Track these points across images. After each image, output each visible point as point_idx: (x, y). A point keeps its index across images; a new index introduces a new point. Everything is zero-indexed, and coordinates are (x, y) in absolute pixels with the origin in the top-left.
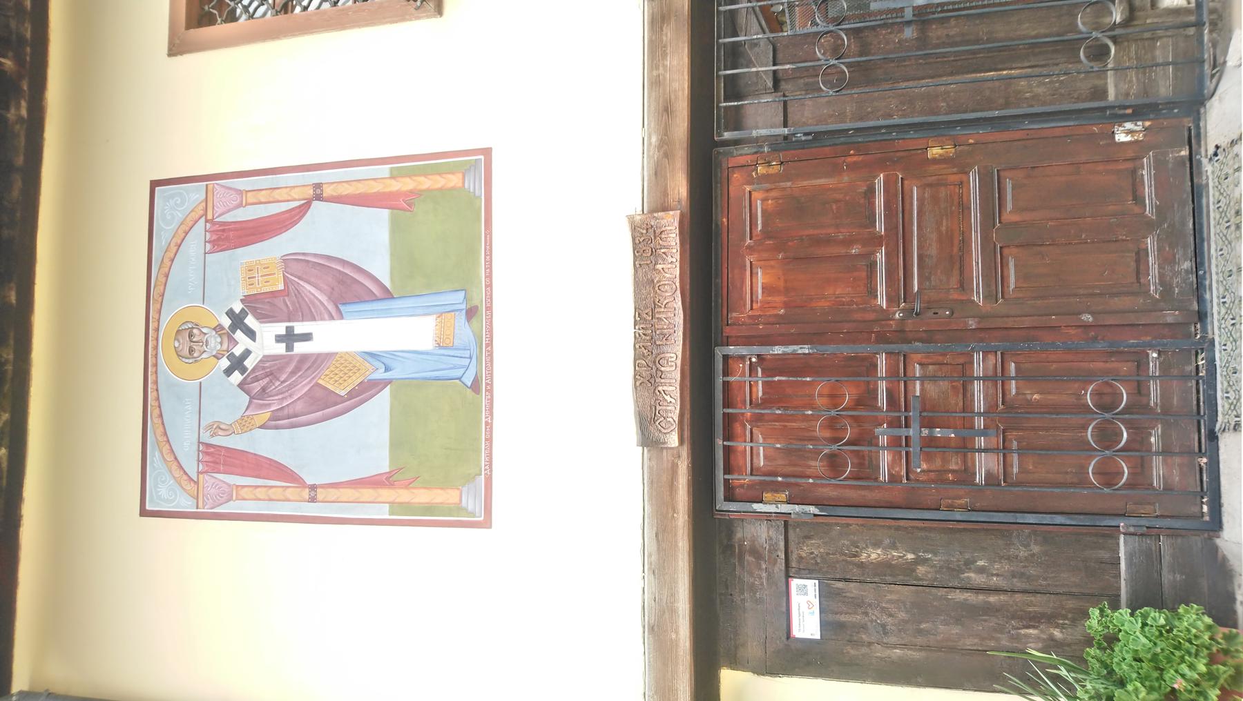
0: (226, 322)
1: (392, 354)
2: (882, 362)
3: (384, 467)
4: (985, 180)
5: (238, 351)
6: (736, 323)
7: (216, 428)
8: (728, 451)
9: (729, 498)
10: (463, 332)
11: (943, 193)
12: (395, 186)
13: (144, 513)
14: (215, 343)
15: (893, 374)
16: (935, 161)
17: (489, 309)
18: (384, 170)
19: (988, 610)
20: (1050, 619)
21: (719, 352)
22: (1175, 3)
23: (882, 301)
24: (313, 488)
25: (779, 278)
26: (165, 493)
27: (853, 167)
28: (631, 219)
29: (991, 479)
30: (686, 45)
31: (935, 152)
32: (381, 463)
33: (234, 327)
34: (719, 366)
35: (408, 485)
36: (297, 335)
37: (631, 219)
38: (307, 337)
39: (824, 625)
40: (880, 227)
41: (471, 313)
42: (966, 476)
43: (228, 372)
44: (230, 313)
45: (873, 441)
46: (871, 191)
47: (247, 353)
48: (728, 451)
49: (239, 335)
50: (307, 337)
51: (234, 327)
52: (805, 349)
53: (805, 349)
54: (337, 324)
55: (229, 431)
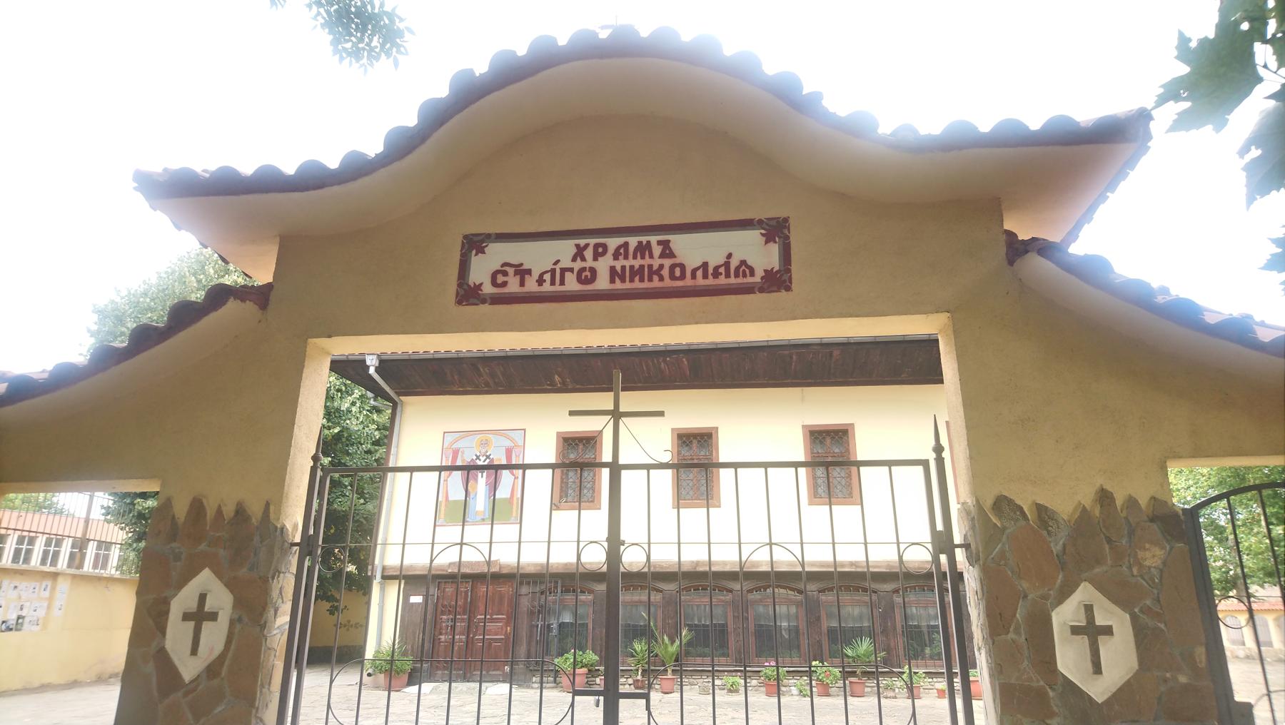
0: (488, 454)
1: (476, 500)
2: (466, 617)
3: (450, 499)
4: (502, 639)
5: (481, 457)
6: (477, 584)
7: (463, 453)
8: (449, 582)
9: (439, 582)
10: (479, 518)
11: (500, 630)
12: (515, 499)
13: (444, 433)
14: (483, 451)
15: (463, 619)
16: (507, 629)
17: (484, 524)
18: (519, 496)
19: (415, 638)
20: (412, 651)
21: (470, 580)
22: (794, 699)
23: (479, 617)
24: (447, 480)
25: (16, 587)
26: (449, 438)
27: (508, 611)
28: (499, 560)
29: (439, 639)
30: (884, 570)
31: (509, 628)
32: (451, 499)
33: (487, 456)
34: (467, 580)
35: (446, 505)
36: (549, 468)
37: (499, 560)
38: (482, 477)
39: (413, 603)
40: (495, 617)
41: (483, 520)
42: (441, 634)
43: (476, 455)
44: (490, 455)
45: (449, 614)
46: (503, 615)
47: (480, 460)
48: (449, 582)
49: (485, 457)
50: (482, 477)
51: (487, 456)
52: (469, 600)
53: (469, 600)
54: (485, 484)
55: (462, 456)
